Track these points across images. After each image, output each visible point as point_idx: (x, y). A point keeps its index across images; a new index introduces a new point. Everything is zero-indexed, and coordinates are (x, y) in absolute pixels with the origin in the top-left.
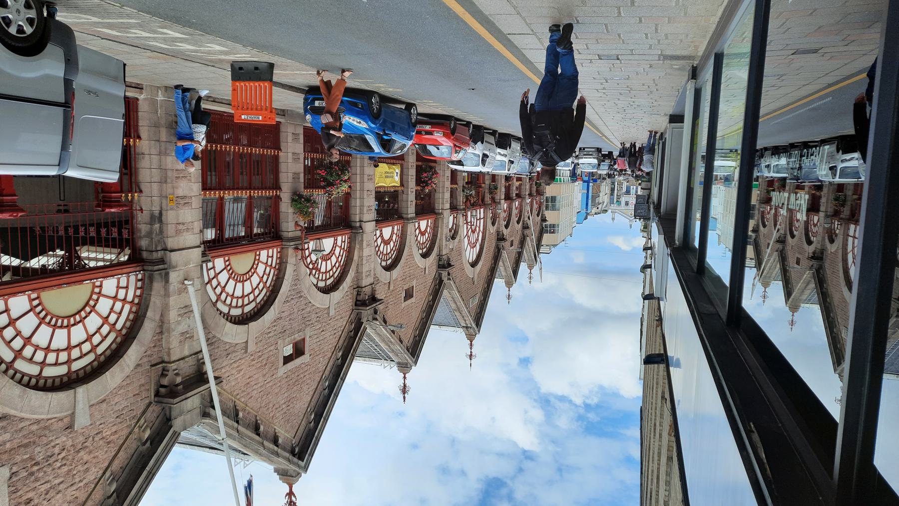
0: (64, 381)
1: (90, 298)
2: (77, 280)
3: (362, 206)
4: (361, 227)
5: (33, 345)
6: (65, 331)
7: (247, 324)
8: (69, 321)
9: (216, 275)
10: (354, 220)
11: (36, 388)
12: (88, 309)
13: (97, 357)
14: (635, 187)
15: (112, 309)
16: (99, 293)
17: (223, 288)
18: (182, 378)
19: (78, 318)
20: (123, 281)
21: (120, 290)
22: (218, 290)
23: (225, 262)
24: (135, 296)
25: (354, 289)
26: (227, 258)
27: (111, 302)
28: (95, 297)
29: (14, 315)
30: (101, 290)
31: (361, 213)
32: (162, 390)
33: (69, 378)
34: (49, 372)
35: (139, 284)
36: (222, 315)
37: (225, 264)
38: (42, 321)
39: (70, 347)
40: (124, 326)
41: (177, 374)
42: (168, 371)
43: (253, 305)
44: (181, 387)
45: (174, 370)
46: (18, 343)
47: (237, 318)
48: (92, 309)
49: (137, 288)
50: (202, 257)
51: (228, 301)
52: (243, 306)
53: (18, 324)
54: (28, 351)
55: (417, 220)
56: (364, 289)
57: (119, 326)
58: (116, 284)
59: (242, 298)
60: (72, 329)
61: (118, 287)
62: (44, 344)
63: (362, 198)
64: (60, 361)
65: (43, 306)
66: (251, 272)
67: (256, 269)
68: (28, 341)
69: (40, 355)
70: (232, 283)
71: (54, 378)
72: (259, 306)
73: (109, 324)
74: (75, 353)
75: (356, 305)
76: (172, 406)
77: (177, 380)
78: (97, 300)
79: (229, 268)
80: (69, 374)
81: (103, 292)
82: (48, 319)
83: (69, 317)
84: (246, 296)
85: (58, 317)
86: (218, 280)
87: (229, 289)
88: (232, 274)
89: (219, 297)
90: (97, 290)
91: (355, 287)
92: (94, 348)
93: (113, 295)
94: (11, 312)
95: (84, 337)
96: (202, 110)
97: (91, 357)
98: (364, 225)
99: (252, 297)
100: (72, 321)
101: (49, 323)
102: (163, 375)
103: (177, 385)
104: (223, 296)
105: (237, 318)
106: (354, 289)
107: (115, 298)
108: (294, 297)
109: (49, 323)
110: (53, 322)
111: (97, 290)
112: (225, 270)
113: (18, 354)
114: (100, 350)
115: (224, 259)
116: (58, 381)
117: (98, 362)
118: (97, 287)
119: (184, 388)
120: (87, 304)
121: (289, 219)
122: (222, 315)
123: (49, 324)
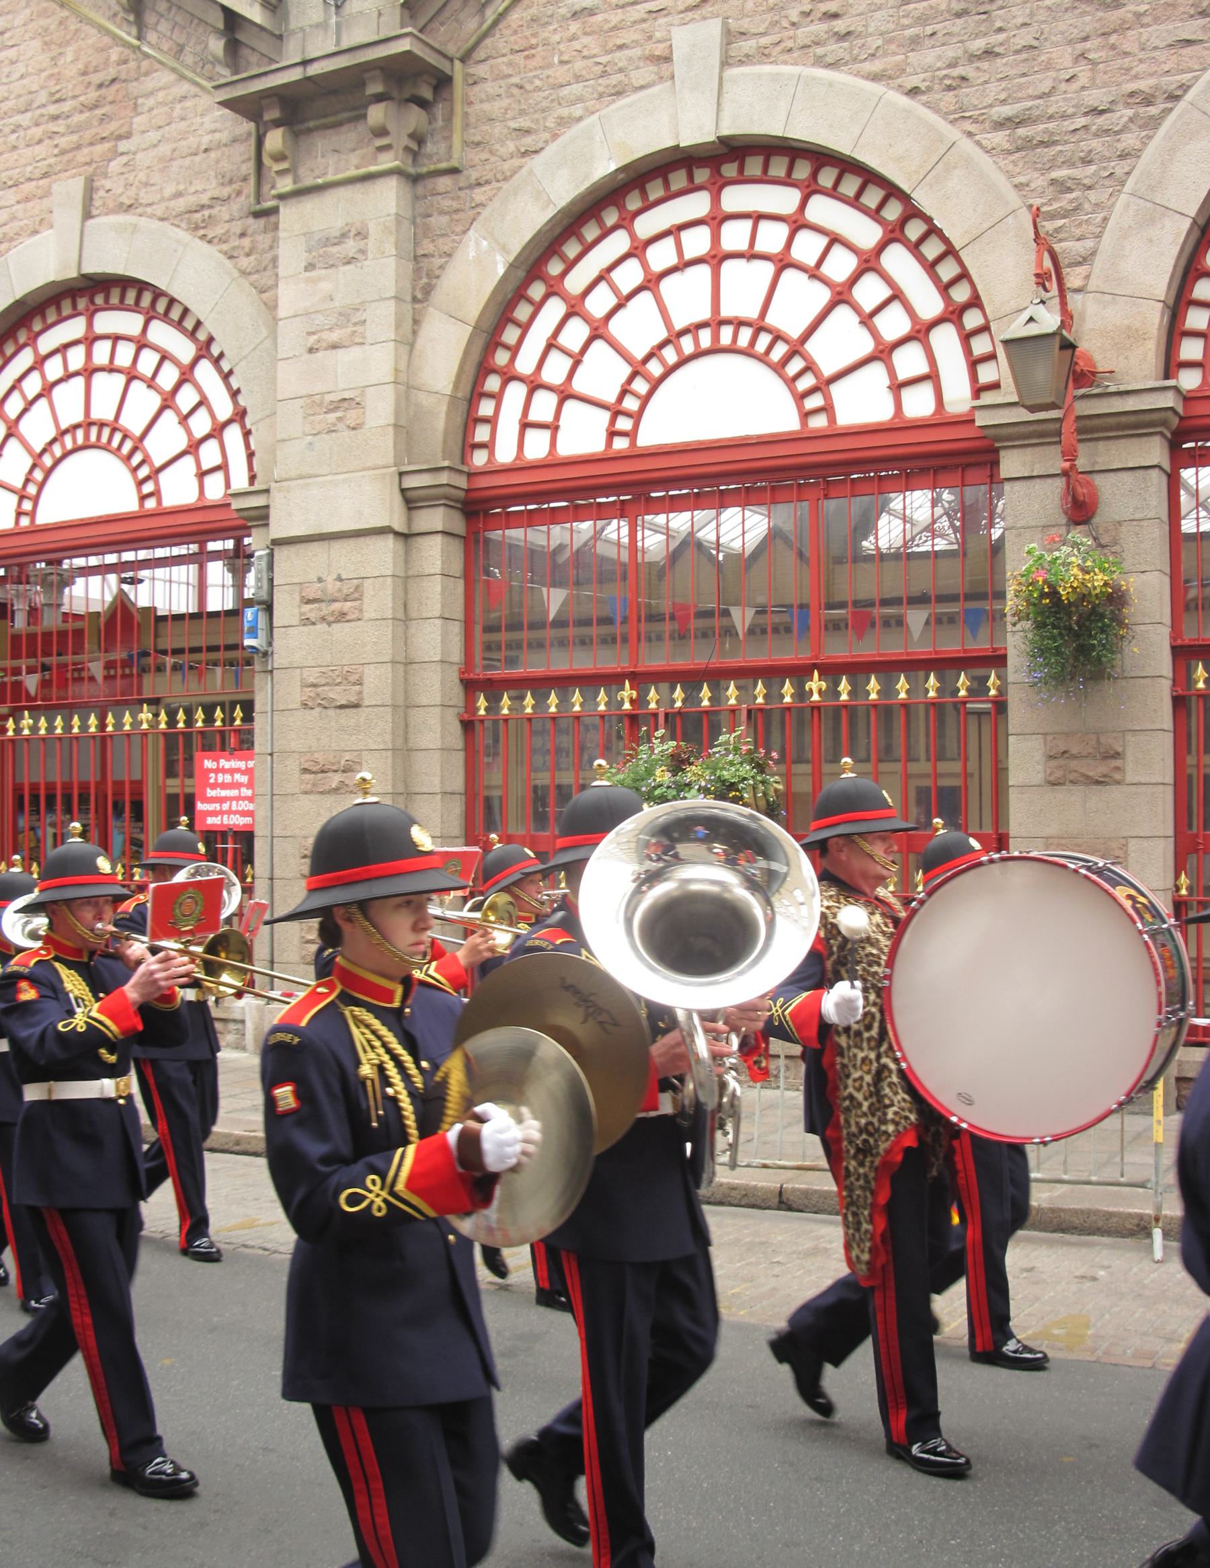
0: (735, 166)
1: (41, 486)
2: (750, 449)
3: (405, 618)
4: (411, 501)
5: (825, 281)
6: (725, 312)
7: (83, 276)
8: (87, 436)
9: (193, 448)
10: (450, 539)
11: (821, 157)
12: (655, 368)
13: (626, 222)
14: (806, 768)
15: (577, 363)
16: (22, 498)
17: (168, 402)
18: (364, 116)
19: (687, 344)
20: (537, 447)
21: (548, 417)
22: (186, 398)
23: (156, 494)
24: (498, 397)
25: (454, 171)
26: (151, 504)
27: (578, 385)
28: (631, 404)
29: (876, 372)
30: (613, 421)
31: (406, 580)
32: (427, 94)
33: (717, 171)
34: (130, 323)
35: (482, 433)
36: (189, 324)
37: (157, 484)
38: (797, 349)
39: (715, 261)
40: (538, 307)
41: (381, 132)
42: (407, 148)
43: (47, 342)
44: (375, 88)
45: (387, 148)
46: (870, 292)
47: (114, 300)
48: (38, 461)
49: (492, 421)
50: (267, 507)
51: (147, 362)
52: (90, 340)
53: (866, 346)
54: (841, 265)
55: (236, 504)
56: (387, 161)
57: (554, 309)
58: (561, 435)
59: (91, 367)
60: (705, 314)
61: (553, 428)
62: (137, 387)
63: (406, 664)
64: (58, 358)
65: (793, 391)
66: (53, 455)
67: (34, 466)
68: (841, 296)
69: (147, 362)
70: (134, 422)
71: (122, 307)
72: (22, 338)
73: (587, 318)
74: (76, 358)
75: (443, 82)
76: (415, 32)
77: (280, 141)
78: (624, 392)
79: (143, 472)
80: (719, 184)
81: (606, 416)
82: (780, 350)
83: (715, 350)
84: (76, 374)
85: (748, 352)
86: (189, 432)
87: (143, 402)
88: (134, 450)
89: (187, 375)
90: (624, 424)
91: (444, 183)
92: (39, 363)
93: (570, 405)
94: (887, 382)
95: (667, 286)
96: (508, 952)
97: (646, 225)
98: (390, 513)
99: (54, 369)
100: (705, 338)
101: (125, 437)
102: (418, 139)
103: (379, 98)
104: (168, 378)
105: (114, 300)
106: (454, 171)
107: (565, 394)
108: (1081, 121)
109: (125, 437)
110: (118, 437)
111: (27, 506)
112: (158, 463)
113: (869, 263)
114: (618, 243)
115: (159, 502)
116: (67, 309)
117: (624, 206)
118: (26, 514)
119: (362, 85)
120: (48, 473)
121: (439, 588)
122: (189, 324)
123: (778, 337)
